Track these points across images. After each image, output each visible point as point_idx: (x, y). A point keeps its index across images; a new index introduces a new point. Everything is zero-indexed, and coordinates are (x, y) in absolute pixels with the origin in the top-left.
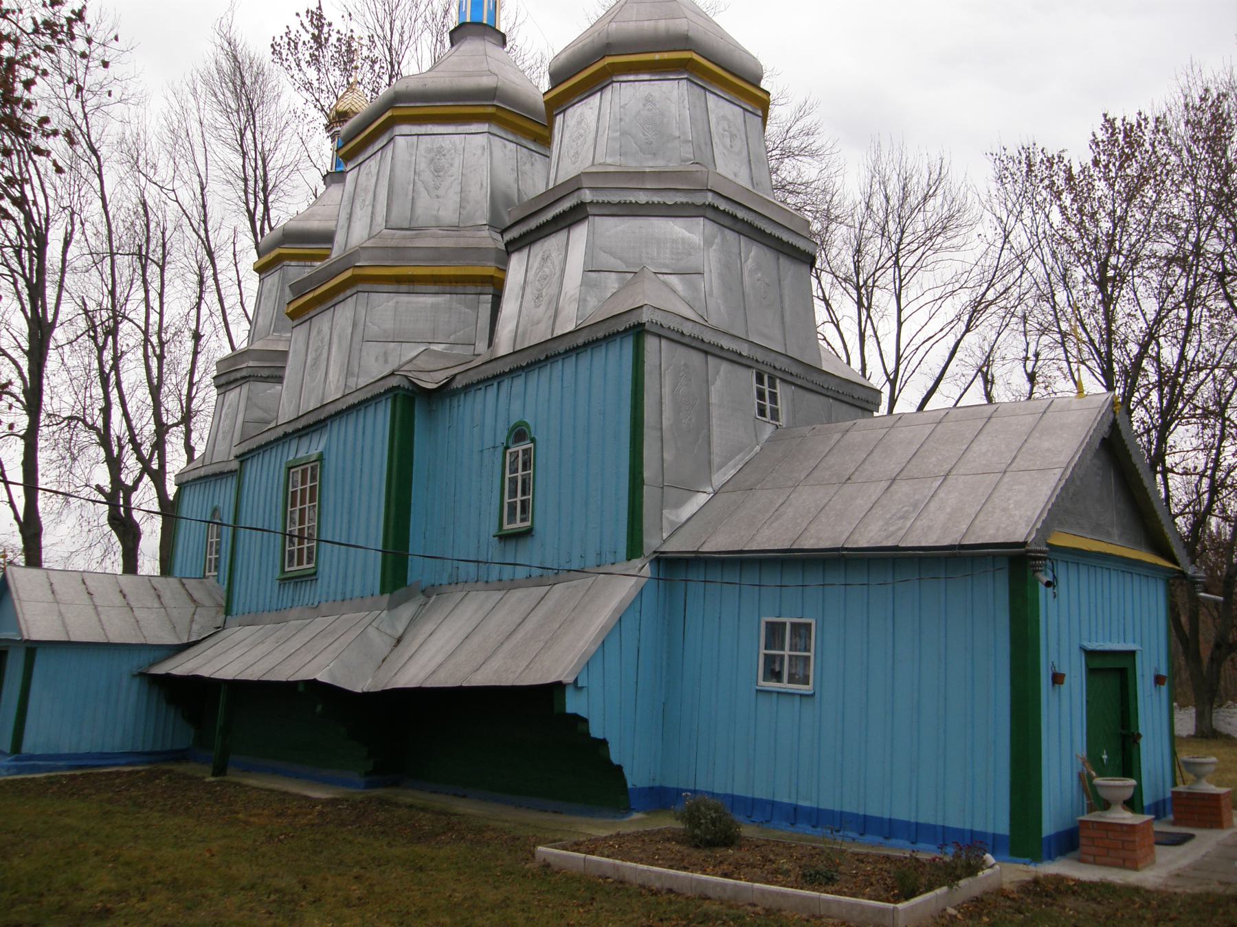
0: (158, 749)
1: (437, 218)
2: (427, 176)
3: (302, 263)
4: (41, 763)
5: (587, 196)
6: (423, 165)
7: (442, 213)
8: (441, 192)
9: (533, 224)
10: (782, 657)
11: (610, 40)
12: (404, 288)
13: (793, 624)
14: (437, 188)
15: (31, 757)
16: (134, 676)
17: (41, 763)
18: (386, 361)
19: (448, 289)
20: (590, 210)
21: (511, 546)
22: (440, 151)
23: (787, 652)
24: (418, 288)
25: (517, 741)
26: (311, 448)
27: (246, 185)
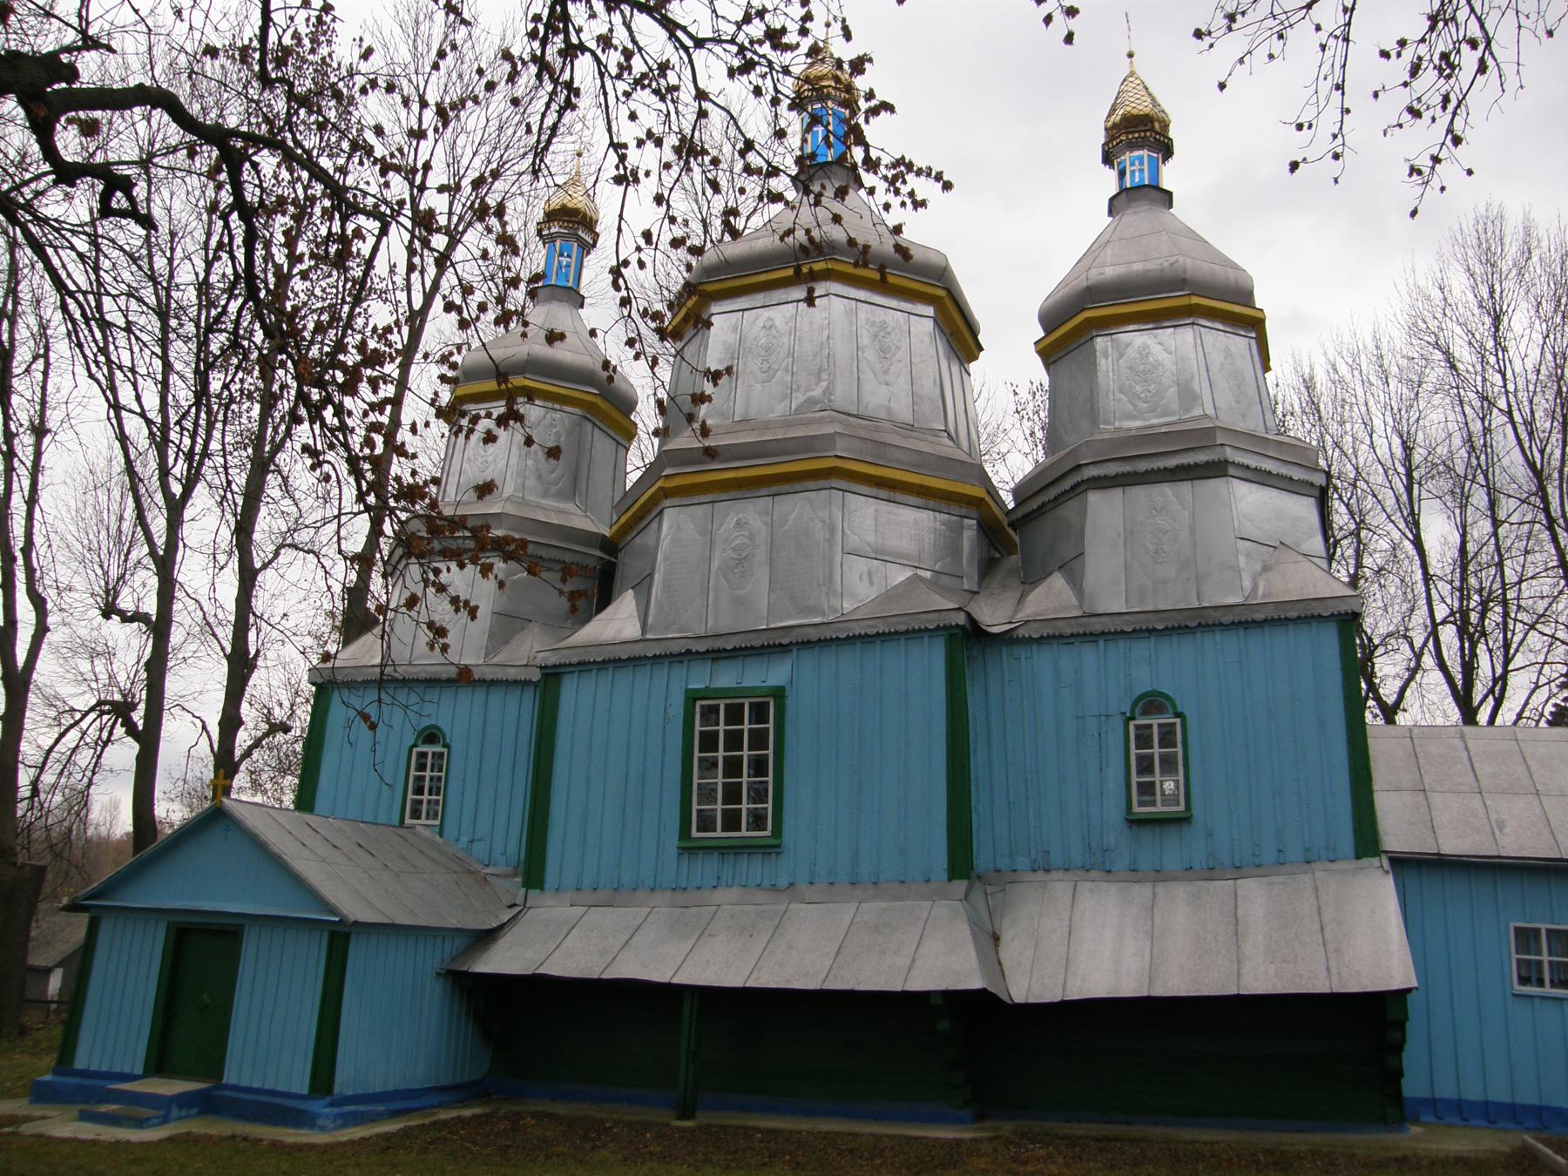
0: (457, 1081)
1: (889, 410)
2: (870, 355)
3: (550, 405)
4: (362, 1108)
5: (1231, 455)
6: (865, 340)
7: (894, 405)
8: (890, 378)
9: (1142, 466)
10: (1539, 963)
11: (1188, 276)
12: (883, 493)
13: (1549, 931)
14: (886, 373)
15: (347, 1100)
16: (438, 974)
17: (362, 1108)
18: (871, 583)
19: (932, 503)
20: (1231, 471)
21: (1146, 834)
22: (883, 326)
23: (1545, 958)
24: (899, 497)
25: (1339, 1046)
26: (775, 674)
27: (1504, 380)
